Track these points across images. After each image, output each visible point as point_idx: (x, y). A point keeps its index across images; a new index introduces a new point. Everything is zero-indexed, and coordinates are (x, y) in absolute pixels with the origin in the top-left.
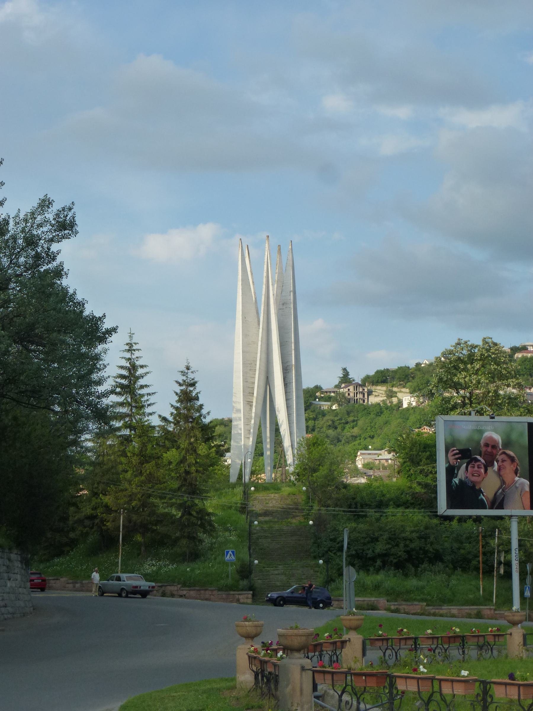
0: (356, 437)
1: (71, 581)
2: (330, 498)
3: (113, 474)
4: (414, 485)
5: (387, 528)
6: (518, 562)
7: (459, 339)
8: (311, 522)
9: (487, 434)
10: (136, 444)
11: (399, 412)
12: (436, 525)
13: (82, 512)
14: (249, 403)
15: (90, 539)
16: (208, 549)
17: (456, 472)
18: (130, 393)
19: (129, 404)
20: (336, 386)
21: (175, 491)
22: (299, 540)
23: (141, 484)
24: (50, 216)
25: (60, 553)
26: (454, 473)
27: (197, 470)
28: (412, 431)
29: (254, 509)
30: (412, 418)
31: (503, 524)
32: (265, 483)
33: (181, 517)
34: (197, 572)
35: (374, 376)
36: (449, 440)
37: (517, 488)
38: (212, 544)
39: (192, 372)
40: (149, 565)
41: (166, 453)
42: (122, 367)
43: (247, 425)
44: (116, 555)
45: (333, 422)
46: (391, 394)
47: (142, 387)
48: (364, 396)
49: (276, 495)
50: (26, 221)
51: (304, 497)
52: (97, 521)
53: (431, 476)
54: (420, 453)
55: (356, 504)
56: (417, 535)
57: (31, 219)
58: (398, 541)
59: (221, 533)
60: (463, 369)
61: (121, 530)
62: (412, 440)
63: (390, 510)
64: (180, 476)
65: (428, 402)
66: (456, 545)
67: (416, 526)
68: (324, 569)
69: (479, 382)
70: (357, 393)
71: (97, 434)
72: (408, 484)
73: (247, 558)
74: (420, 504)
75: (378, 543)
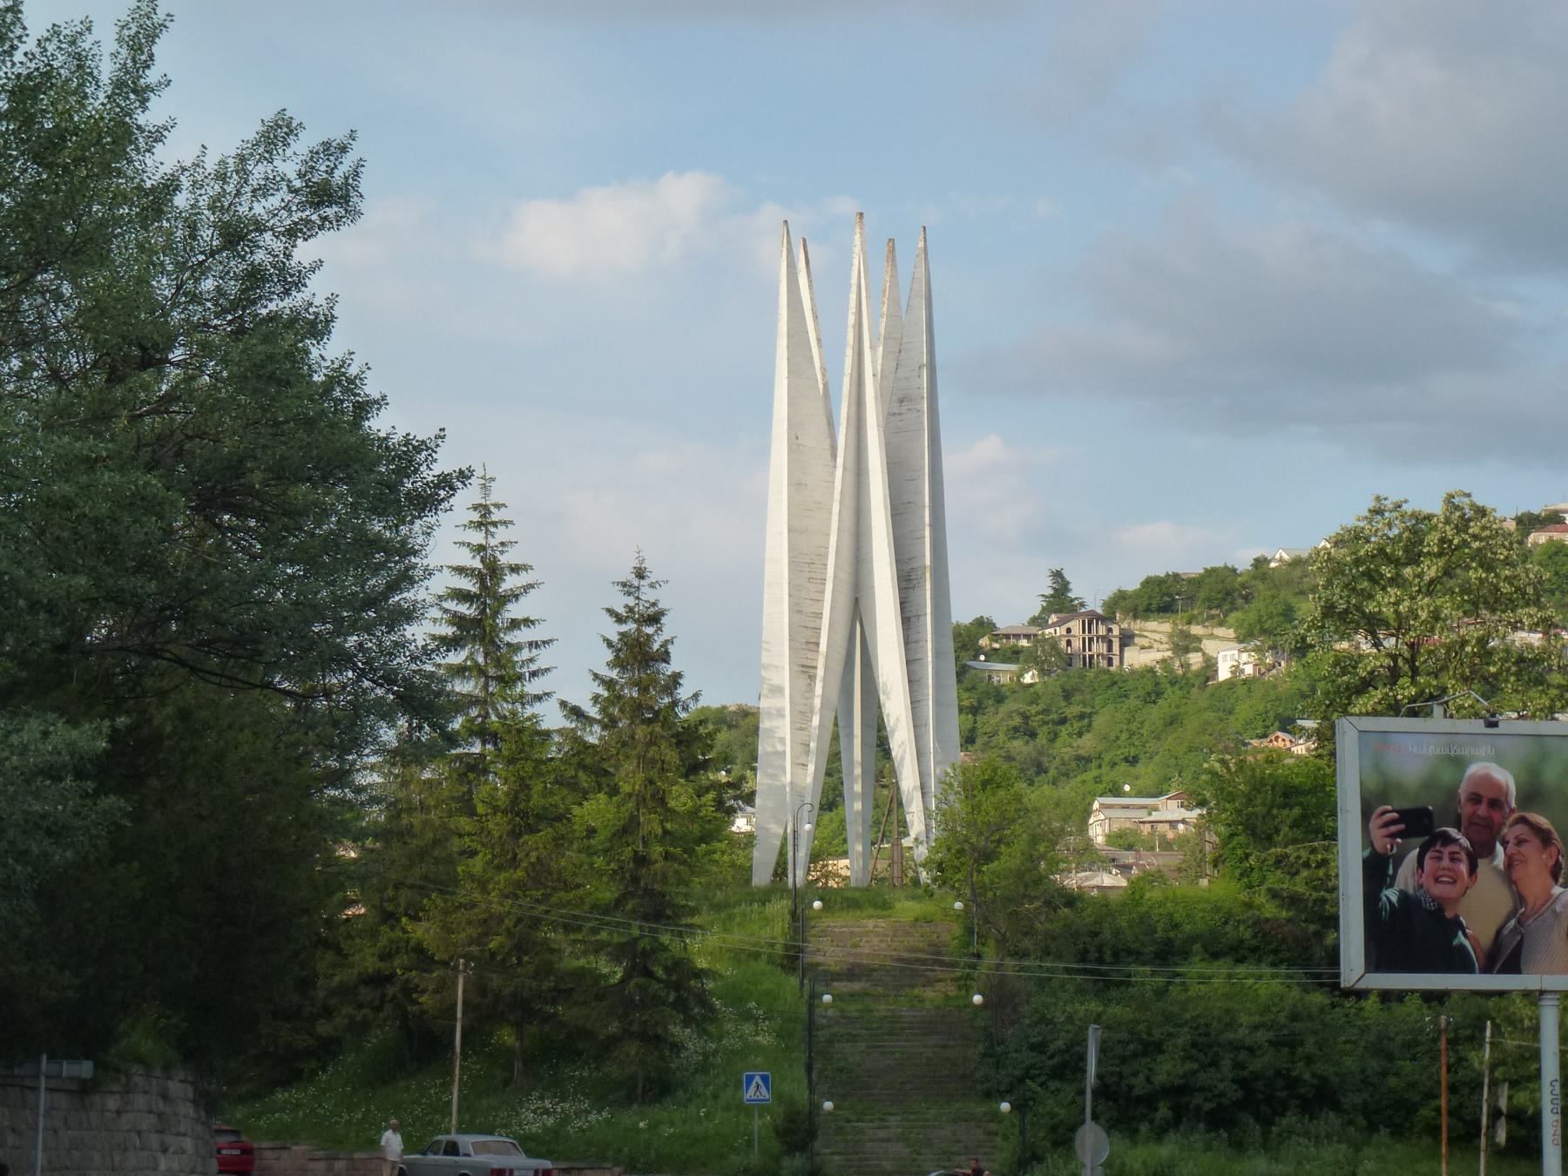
0: (1088, 760)
1: (320, 1154)
2: (1029, 932)
3: (437, 861)
4: (1261, 899)
5: (1187, 1016)
6: (1558, 1117)
7: (1378, 499)
8: (977, 999)
9: (1474, 769)
10: (498, 784)
11: (1208, 691)
12: (1322, 1010)
13: (352, 966)
14: (805, 671)
15: (374, 1039)
16: (697, 1071)
17: (1391, 872)
18: (482, 640)
19: (482, 672)
20: (1034, 621)
21: (606, 910)
22: (944, 1047)
23: (514, 892)
24: (288, 167)
25: (292, 1077)
26: (1385, 873)
27: (667, 852)
28: (1245, 744)
29: (819, 958)
30: (1244, 711)
31: (1506, 1009)
32: (847, 888)
33: (622, 981)
34: (668, 1131)
35: (1137, 593)
36: (1372, 784)
37: (1556, 915)
38: (706, 1056)
39: (652, 586)
40: (534, 1112)
41: (580, 804)
42: (460, 570)
43: (801, 729)
44: (442, 1085)
45: (1026, 717)
46: (1185, 644)
47: (515, 624)
48: (1110, 649)
49: (881, 923)
50: (222, 177)
51: (958, 930)
52: (391, 991)
53: (1305, 873)
54: (1275, 811)
55: (1100, 950)
56: (1270, 1035)
57: (237, 172)
58: (1216, 1054)
59: (729, 1026)
60: (1392, 579)
61: (459, 1015)
62: (1253, 776)
63: (1195, 967)
64: (621, 868)
65: (1288, 666)
66: (1374, 1065)
67: (1267, 1009)
68: (1013, 1125)
69: (1436, 616)
70: (1091, 640)
71: (395, 753)
72: (1243, 896)
73: (802, 1095)
74: (1275, 952)
75: (1160, 1058)
